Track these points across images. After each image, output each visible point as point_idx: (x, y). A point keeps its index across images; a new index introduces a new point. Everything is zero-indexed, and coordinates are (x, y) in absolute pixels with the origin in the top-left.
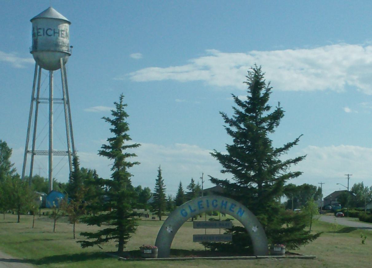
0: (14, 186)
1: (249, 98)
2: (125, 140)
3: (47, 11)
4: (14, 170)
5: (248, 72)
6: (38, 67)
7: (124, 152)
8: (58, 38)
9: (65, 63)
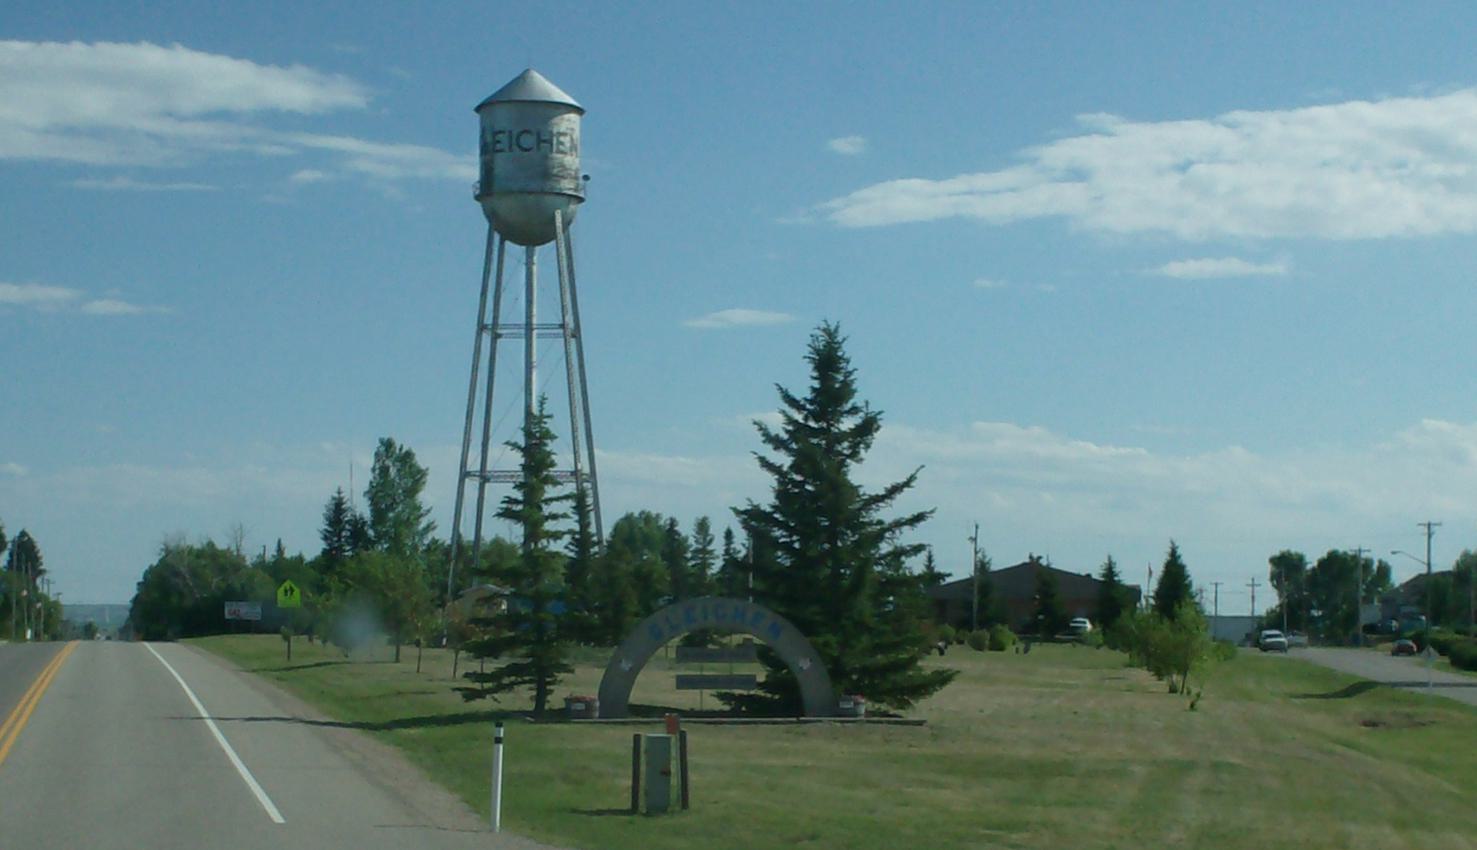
0: (386, 573)
1: (814, 390)
2: (550, 486)
3: (522, 79)
4: (429, 528)
5: (812, 336)
6: (497, 237)
7: (547, 510)
8: (550, 156)
9: (567, 224)
